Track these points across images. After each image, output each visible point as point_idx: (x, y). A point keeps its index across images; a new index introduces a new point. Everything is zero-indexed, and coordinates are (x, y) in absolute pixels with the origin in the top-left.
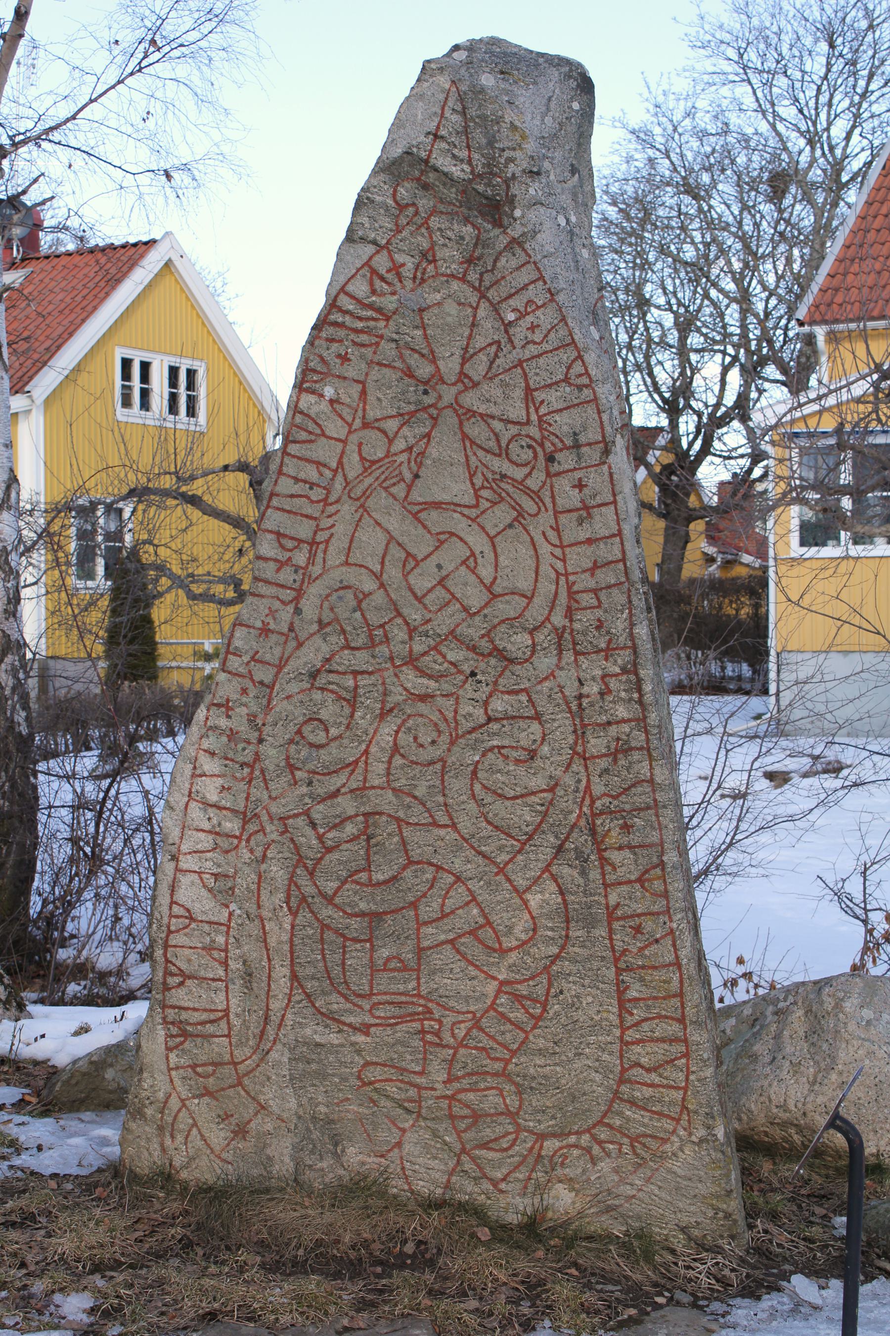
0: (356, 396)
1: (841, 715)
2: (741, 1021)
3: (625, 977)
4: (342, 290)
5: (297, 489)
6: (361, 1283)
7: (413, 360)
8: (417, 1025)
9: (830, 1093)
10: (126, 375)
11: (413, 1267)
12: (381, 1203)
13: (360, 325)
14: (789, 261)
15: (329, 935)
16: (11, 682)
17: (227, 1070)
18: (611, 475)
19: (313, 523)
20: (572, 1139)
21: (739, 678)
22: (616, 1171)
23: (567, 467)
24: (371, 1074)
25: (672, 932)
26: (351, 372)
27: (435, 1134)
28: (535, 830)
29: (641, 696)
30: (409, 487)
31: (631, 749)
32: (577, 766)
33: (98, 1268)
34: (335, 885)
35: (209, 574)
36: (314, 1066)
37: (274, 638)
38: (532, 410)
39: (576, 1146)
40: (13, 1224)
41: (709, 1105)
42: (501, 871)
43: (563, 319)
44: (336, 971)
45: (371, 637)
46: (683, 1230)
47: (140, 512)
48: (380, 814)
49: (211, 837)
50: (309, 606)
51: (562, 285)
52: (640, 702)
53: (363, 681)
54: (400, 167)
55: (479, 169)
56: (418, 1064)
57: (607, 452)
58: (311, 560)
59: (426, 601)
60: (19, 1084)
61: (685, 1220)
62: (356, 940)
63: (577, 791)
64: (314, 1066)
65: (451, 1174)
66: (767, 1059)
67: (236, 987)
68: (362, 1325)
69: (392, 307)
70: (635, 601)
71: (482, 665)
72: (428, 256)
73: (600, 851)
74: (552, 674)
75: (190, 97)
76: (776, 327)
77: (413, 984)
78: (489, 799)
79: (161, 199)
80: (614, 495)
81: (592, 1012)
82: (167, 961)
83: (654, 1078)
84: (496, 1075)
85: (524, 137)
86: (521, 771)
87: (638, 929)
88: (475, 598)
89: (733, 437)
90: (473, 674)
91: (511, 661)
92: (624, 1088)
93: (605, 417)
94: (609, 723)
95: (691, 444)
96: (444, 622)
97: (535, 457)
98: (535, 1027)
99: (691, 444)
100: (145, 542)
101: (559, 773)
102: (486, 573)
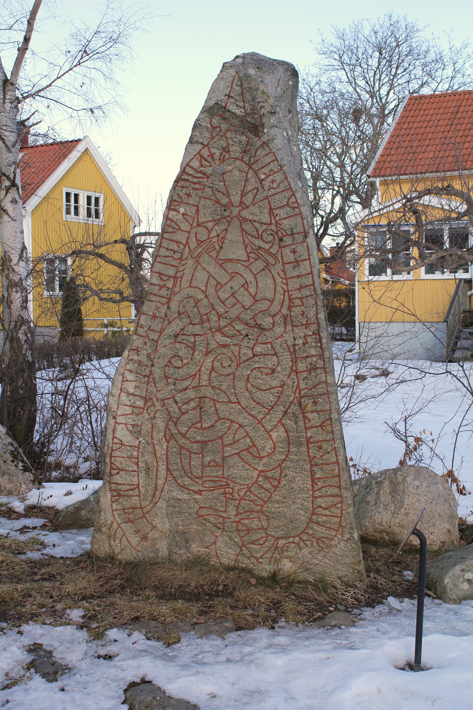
0: (194, 212)
1: (396, 351)
2: (361, 487)
3: (315, 468)
4: (188, 165)
5: (168, 253)
6: (201, 604)
7: (220, 196)
8: (222, 490)
9: (401, 518)
10: (68, 200)
11: (222, 596)
12: (207, 568)
13: (196, 180)
14: (362, 149)
15: (184, 451)
16: (25, 338)
17: (139, 511)
18: (308, 247)
19: (175, 269)
20: (291, 539)
21: (341, 334)
22: (310, 553)
23: (288, 243)
24: (202, 512)
25: (335, 448)
26: (192, 201)
27: (231, 538)
28: (275, 404)
29: (321, 345)
30: (218, 253)
31: (317, 368)
32: (293, 376)
33: (84, 598)
34: (186, 429)
35: (108, 289)
36: (177, 509)
37: (158, 320)
38: (272, 218)
39: (293, 542)
40: (46, 579)
41: (351, 524)
42: (260, 422)
43: (286, 178)
44: (187, 467)
45: (201, 319)
46: (339, 578)
47: (77, 262)
48: (206, 397)
49: (131, 408)
50: (174, 305)
51: (286, 163)
52: (321, 347)
53: (198, 338)
54: (214, 111)
55: (248, 111)
56: (222, 506)
57: (306, 237)
58: (174, 285)
59: (226, 303)
60: (42, 517)
61: (340, 574)
62: (195, 453)
63: (293, 387)
64: (177, 509)
65: (238, 555)
66: (373, 503)
67: (142, 475)
68: (202, 621)
69: (210, 172)
70: (319, 303)
71: (251, 332)
72: (226, 150)
73: (303, 413)
74: (282, 335)
75: (102, 76)
76: (356, 179)
77: (221, 472)
78: (254, 391)
79: (89, 122)
80: (309, 256)
81: (300, 484)
82: (112, 463)
83: (327, 512)
84: (257, 512)
85: (268, 97)
86: (268, 378)
87: (320, 448)
88: (248, 301)
89: (338, 227)
90: (247, 335)
91: (264, 330)
92: (314, 517)
93: (305, 221)
94: (307, 357)
95: (318, 230)
96: (234, 313)
97: (274, 239)
98: (274, 491)
99: (318, 230)
100: (79, 275)
101: (285, 379)
102: (252, 290)
